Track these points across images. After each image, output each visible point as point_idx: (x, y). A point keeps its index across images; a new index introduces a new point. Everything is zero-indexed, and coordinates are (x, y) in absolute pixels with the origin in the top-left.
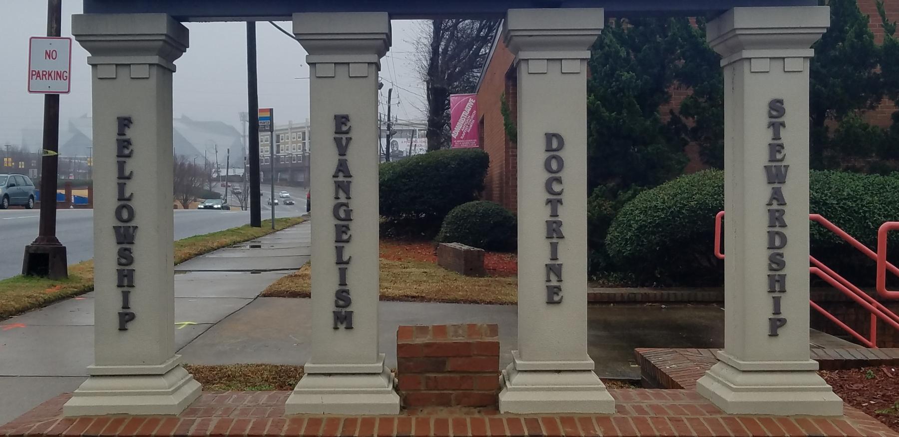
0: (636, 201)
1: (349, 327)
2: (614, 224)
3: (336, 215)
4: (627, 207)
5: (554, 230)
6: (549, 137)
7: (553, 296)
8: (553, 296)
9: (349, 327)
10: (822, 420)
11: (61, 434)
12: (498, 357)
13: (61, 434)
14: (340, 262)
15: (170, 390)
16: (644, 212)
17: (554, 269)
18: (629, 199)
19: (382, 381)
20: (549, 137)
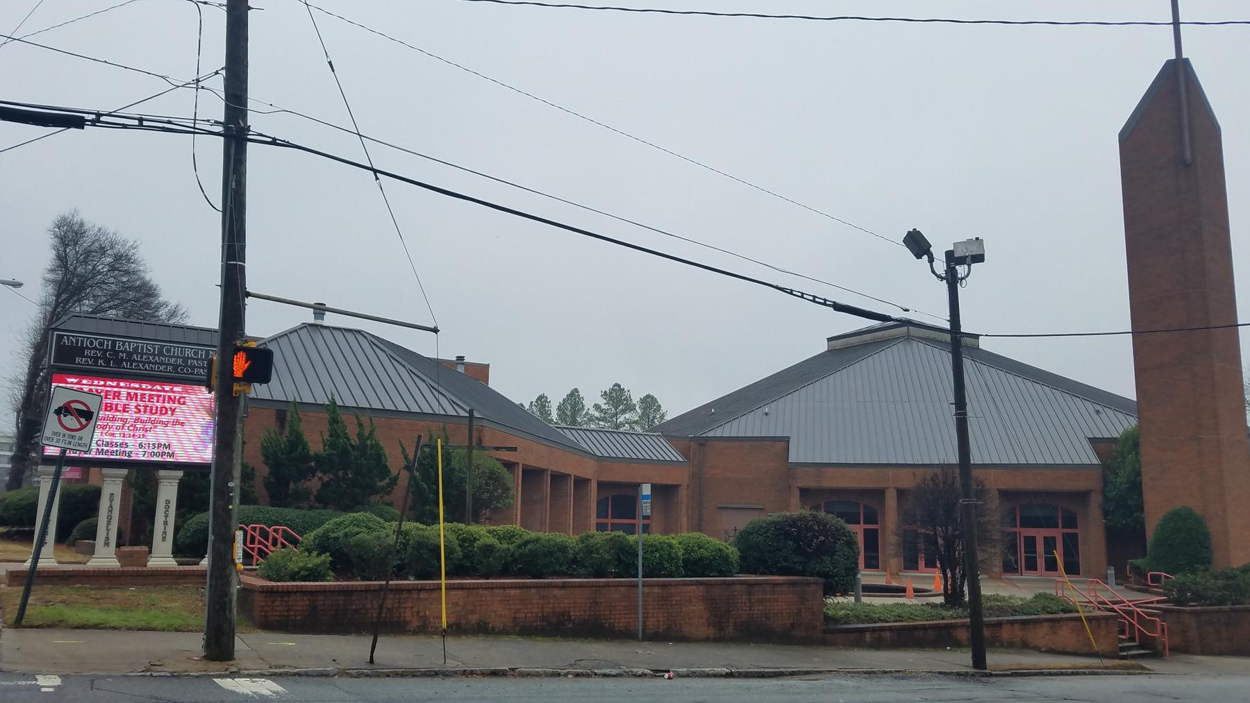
0: (194, 519)
1: (108, 546)
2: (182, 529)
3: (107, 518)
4: (189, 522)
5: (166, 523)
6: (166, 501)
7: (164, 539)
8: (164, 539)
9: (108, 546)
10: (174, 568)
11: (1056, 550)
12: (703, 631)
13: (1056, 550)
14: (107, 530)
15: (1148, 618)
16: (197, 524)
17: (165, 533)
18: (191, 518)
19: (53, 560)
20: (166, 501)
